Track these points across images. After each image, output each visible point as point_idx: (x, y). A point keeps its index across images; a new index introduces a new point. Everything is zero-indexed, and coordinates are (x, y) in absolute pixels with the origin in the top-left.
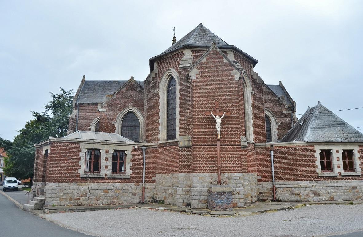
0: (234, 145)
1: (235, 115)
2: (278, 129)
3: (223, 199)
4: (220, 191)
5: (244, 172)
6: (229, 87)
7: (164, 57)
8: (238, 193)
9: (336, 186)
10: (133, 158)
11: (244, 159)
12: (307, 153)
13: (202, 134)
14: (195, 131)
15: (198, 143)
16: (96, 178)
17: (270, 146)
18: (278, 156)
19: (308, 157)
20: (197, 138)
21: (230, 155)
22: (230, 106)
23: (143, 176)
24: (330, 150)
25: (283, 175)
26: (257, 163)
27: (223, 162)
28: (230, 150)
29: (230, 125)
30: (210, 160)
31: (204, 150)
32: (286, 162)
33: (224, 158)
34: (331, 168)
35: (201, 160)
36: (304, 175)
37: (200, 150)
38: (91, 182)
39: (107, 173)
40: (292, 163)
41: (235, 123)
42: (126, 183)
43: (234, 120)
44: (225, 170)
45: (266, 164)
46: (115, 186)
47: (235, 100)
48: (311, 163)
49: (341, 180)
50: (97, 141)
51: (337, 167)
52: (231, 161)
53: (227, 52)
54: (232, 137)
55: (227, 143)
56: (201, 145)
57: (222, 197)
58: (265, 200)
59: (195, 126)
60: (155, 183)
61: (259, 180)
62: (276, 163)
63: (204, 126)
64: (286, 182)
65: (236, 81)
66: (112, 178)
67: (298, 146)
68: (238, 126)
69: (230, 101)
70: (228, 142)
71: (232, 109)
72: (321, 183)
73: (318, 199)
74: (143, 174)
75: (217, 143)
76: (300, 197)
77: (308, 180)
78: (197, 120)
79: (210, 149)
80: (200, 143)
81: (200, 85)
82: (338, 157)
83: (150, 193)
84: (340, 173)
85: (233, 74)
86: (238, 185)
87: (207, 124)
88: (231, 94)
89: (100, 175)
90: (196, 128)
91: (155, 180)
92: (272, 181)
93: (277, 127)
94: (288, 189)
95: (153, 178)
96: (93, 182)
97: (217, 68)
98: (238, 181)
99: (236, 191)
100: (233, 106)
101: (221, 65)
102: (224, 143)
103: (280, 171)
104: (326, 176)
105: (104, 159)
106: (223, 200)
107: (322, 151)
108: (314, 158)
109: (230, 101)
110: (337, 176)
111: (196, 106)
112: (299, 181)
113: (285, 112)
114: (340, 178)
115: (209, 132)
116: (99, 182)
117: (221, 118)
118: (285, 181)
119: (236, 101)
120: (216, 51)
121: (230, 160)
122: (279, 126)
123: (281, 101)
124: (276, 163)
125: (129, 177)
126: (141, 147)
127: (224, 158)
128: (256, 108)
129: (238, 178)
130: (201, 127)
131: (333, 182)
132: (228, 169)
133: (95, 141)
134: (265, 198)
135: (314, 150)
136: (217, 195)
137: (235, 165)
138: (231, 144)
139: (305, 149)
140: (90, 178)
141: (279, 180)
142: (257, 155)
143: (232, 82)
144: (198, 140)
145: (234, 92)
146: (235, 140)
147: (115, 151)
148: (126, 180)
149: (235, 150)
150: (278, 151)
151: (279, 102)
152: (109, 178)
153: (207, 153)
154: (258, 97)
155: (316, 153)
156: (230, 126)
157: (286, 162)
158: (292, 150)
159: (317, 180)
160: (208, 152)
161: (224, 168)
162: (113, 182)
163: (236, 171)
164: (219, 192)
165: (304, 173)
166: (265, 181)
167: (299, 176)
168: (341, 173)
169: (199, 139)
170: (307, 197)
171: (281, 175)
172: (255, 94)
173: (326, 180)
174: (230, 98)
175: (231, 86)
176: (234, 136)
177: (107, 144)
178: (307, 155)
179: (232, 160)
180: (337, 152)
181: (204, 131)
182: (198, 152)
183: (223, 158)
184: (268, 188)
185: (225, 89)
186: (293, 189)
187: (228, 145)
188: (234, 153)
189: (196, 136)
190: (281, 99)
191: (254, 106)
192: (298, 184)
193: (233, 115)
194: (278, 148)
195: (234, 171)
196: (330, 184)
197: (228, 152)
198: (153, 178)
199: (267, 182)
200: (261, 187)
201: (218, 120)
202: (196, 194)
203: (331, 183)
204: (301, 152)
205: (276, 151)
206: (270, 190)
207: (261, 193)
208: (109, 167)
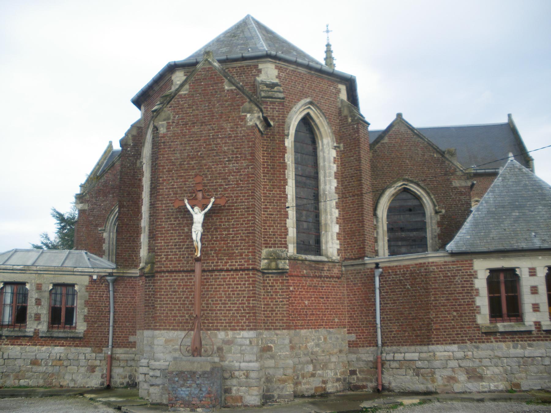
0: (241, 270)
1: (244, 202)
2: (439, 224)
3: (190, 386)
4: (184, 370)
5: (279, 329)
6: (234, 142)
7: (151, 93)
8: (244, 374)
9: (526, 355)
10: (89, 299)
11: (279, 298)
12: (454, 279)
13: (173, 249)
14: (159, 243)
15: (164, 267)
16: (18, 337)
17: (374, 266)
18: (390, 289)
19: (458, 287)
20: (163, 256)
21: (231, 291)
22: (235, 184)
23: (109, 334)
24: (512, 271)
25: (400, 331)
26: (348, 306)
27: (216, 307)
28: (231, 280)
29: (233, 225)
30: (189, 304)
31: (177, 282)
32: (406, 302)
33: (218, 297)
34: (518, 312)
35: (169, 304)
36: (445, 332)
37: (167, 283)
38: (8, 345)
39: (39, 327)
40: (419, 304)
41: (244, 221)
42: (75, 346)
43: (242, 215)
44: (219, 325)
45: (365, 308)
46: (53, 352)
47: (245, 168)
48: (464, 302)
49: (541, 342)
50: (19, 267)
51: (531, 310)
52: (232, 304)
53: (261, 66)
54: (237, 252)
55: (226, 266)
56: (171, 272)
57: (189, 382)
58: (362, 389)
59: (160, 231)
60: (135, 348)
61: (352, 344)
62: (386, 304)
63: (178, 230)
64: (405, 348)
65: (249, 126)
66: (49, 337)
67: (433, 263)
68: (251, 227)
69: (234, 172)
70: (228, 262)
71: (239, 190)
72: (487, 350)
73: (474, 386)
74: (109, 329)
75: (194, 266)
76: (433, 381)
77: (454, 343)
78: (164, 218)
79: (188, 279)
80: (169, 267)
81: (174, 145)
82: (534, 284)
83: (123, 367)
84: (538, 324)
85: (243, 112)
86: (247, 358)
87: (184, 227)
88: (237, 157)
89: (26, 332)
90: (162, 237)
91: (135, 342)
92: (377, 346)
93: (439, 220)
94: (406, 364)
95: (132, 339)
96: (12, 345)
97: (210, 103)
98: (248, 348)
99: (240, 369)
100: (240, 184)
101: (219, 96)
102: (218, 266)
103: (394, 323)
104: (502, 333)
105: (34, 300)
106: (189, 389)
107: (494, 272)
108: (472, 290)
109: (234, 172)
110: (530, 332)
111: (163, 189)
112: (433, 344)
113: (456, 183)
114: (540, 337)
115: (187, 243)
116: (22, 345)
117: (204, 212)
118: (403, 345)
119: (248, 172)
120: (211, 68)
121: (231, 304)
122: (443, 217)
123: (447, 159)
124: (386, 304)
125: (81, 335)
126: (106, 276)
127: (218, 297)
128: (346, 180)
129: (248, 342)
130: (172, 233)
131: (519, 346)
132: (227, 323)
133: (15, 267)
134: (360, 384)
135: (472, 271)
136: (176, 379)
137: (242, 313)
138: (177, 269)
139: (448, 271)
140: (7, 337)
141: (392, 343)
142: (349, 287)
143: (240, 129)
144: (165, 261)
145: (245, 150)
146: (243, 259)
147: (55, 285)
148: (75, 341)
149: (242, 281)
150: (389, 278)
151: (443, 162)
152: (42, 337)
153: (183, 288)
154: (350, 157)
155: (476, 278)
156: (233, 228)
157: (406, 302)
158: (420, 273)
159: (479, 342)
160: (184, 285)
161: (216, 320)
162: (51, 346)
163: (242, 326)
164: (182, 372)
165: (445, 326)
166: (363, 347)
167: (433, 332)
168: (542, 323)
169: (167, 258)
170: (451, 382)
171: (396, 331)
172: (344, 151)
173: (500, 341)
174: (234, 166)
175: (238, 139)
176: (242, 249)
177: (39, 272)
178: (455, 284)
179: (236, 304)
180: (533, 272)
181: (177, 242)
182: (165, 286)
183: (216, 299)
184: (367, 362)
185: (225, 146)
186: (419, 364)
187: (228, 270)
188: (239, 286)
189: (160, 252)
190: (447, 156)
191: (341, 176)
192: (430, 352)
193: (240, 202)
194: (390, 271)
195: (238, 326)
196: (513, 351)
197: (226, 285)
198: (132, 339)
199: (368, 348)
200: (353, 360)
201: (198, 216)
202: (158, 373)
203: (514, 348)
204: (440, 277)
205: (386, 278)
206: (371, 365)
207: (353, 372)
208: (42, 316)
